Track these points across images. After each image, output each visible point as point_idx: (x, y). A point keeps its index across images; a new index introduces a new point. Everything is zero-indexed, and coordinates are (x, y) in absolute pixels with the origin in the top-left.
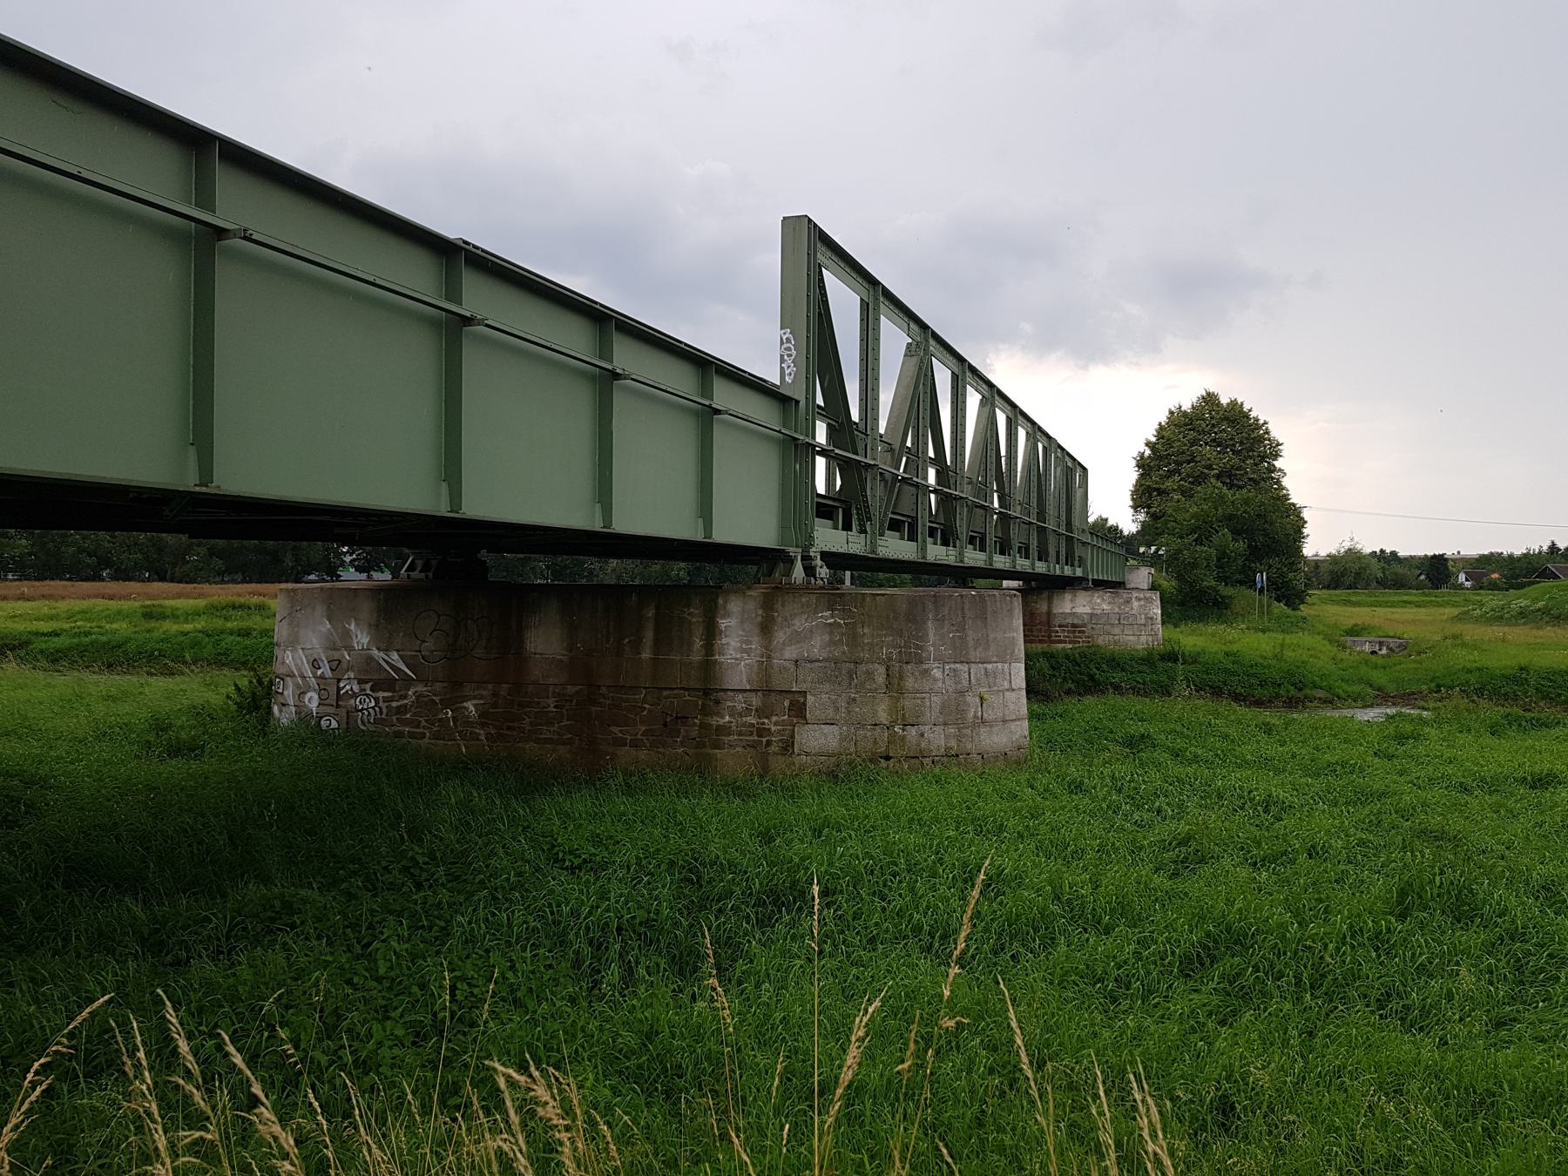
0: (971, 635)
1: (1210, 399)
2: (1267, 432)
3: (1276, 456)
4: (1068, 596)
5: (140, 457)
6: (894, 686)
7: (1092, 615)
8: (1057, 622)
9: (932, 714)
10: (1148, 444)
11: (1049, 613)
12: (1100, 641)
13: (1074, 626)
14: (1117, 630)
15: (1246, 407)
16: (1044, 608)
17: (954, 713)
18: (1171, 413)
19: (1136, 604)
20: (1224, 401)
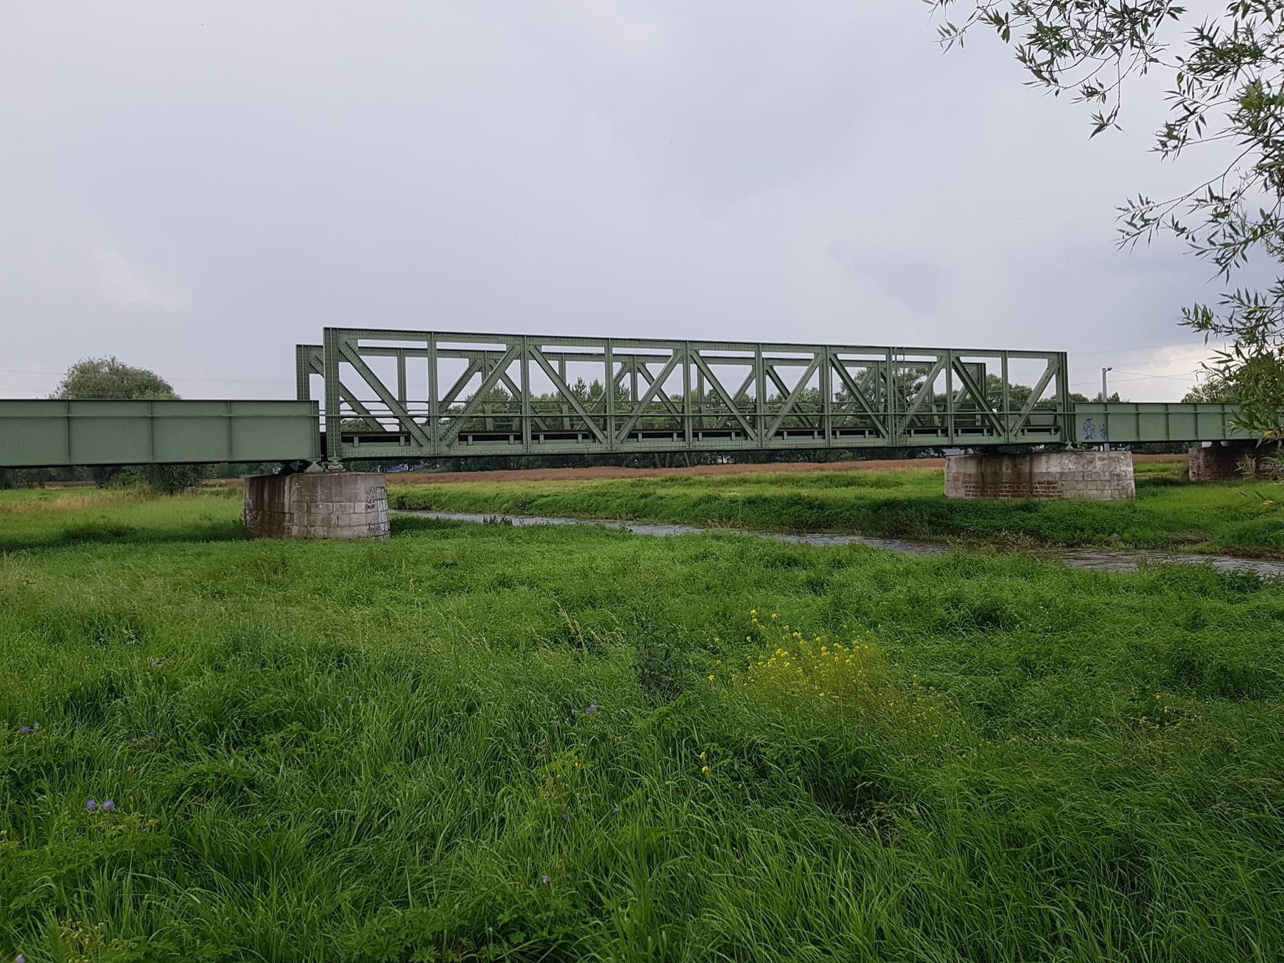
0: (334, 492)
4: (1044, 458)
5: (55, 456)
6: (309, 512)
7: (1062, 474)
8: (1036, 480)
9: (319, 523)
11: (1031, 473)
12: (1068, 495)
13: (1049, 483)
14: (1081, 486)
16: (1027, 470)
17: (327, 522)
19: (1098, 464)
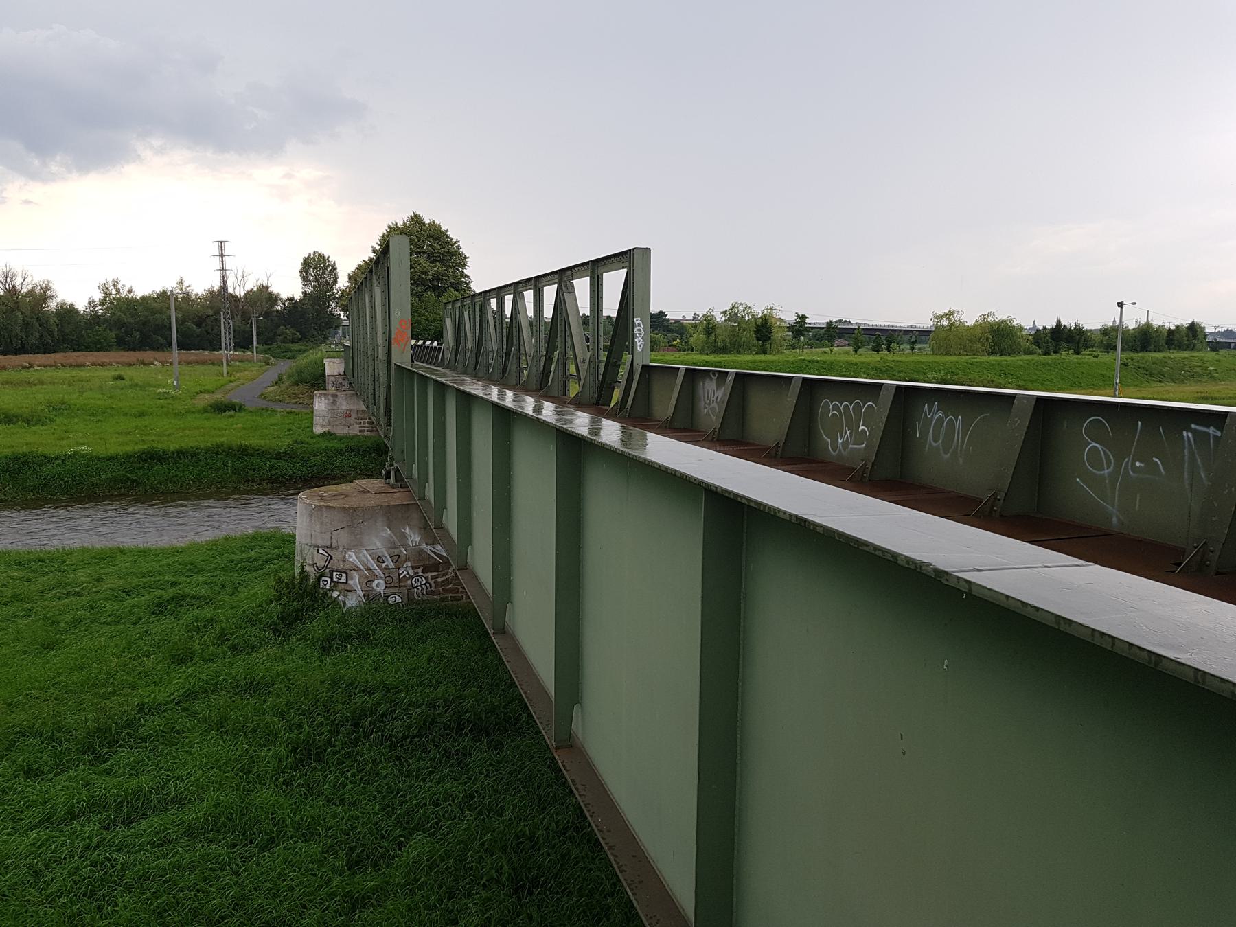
1: (416, 219)
2: (459, 248)
3: (464, 265)
10: (374, 251)
15: (443, 229)
18: (390, 227)
20: (427, 221)
